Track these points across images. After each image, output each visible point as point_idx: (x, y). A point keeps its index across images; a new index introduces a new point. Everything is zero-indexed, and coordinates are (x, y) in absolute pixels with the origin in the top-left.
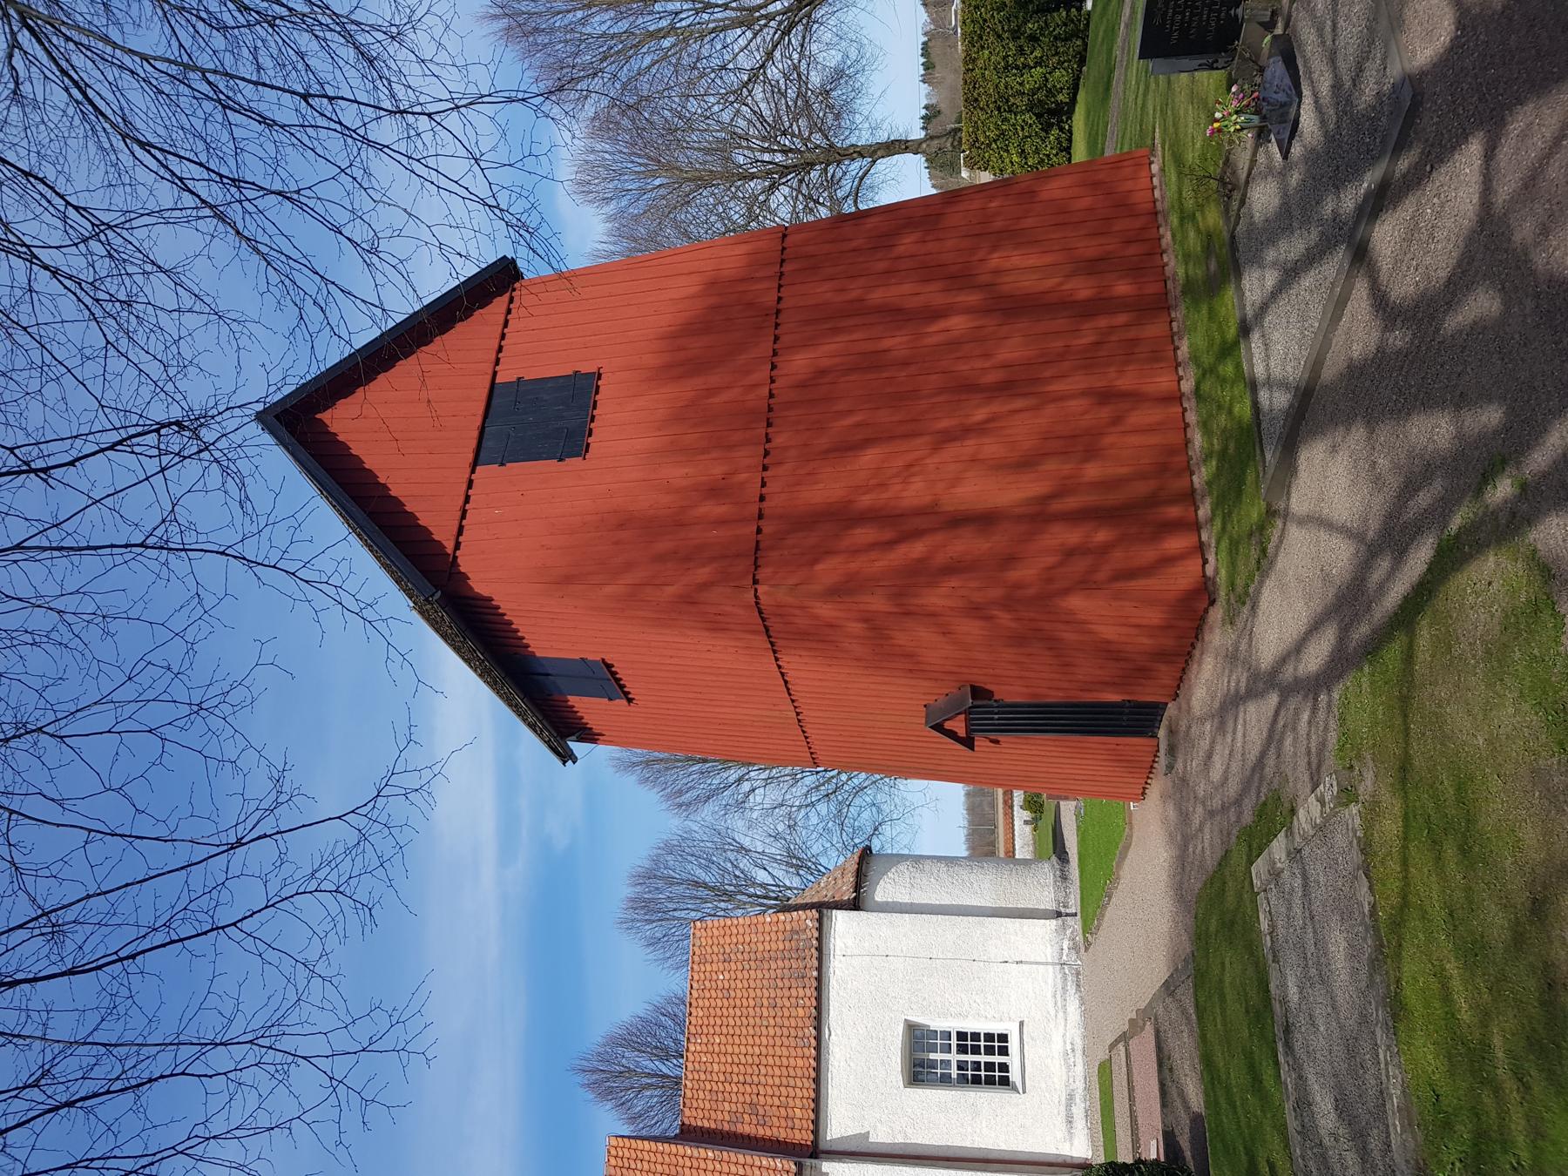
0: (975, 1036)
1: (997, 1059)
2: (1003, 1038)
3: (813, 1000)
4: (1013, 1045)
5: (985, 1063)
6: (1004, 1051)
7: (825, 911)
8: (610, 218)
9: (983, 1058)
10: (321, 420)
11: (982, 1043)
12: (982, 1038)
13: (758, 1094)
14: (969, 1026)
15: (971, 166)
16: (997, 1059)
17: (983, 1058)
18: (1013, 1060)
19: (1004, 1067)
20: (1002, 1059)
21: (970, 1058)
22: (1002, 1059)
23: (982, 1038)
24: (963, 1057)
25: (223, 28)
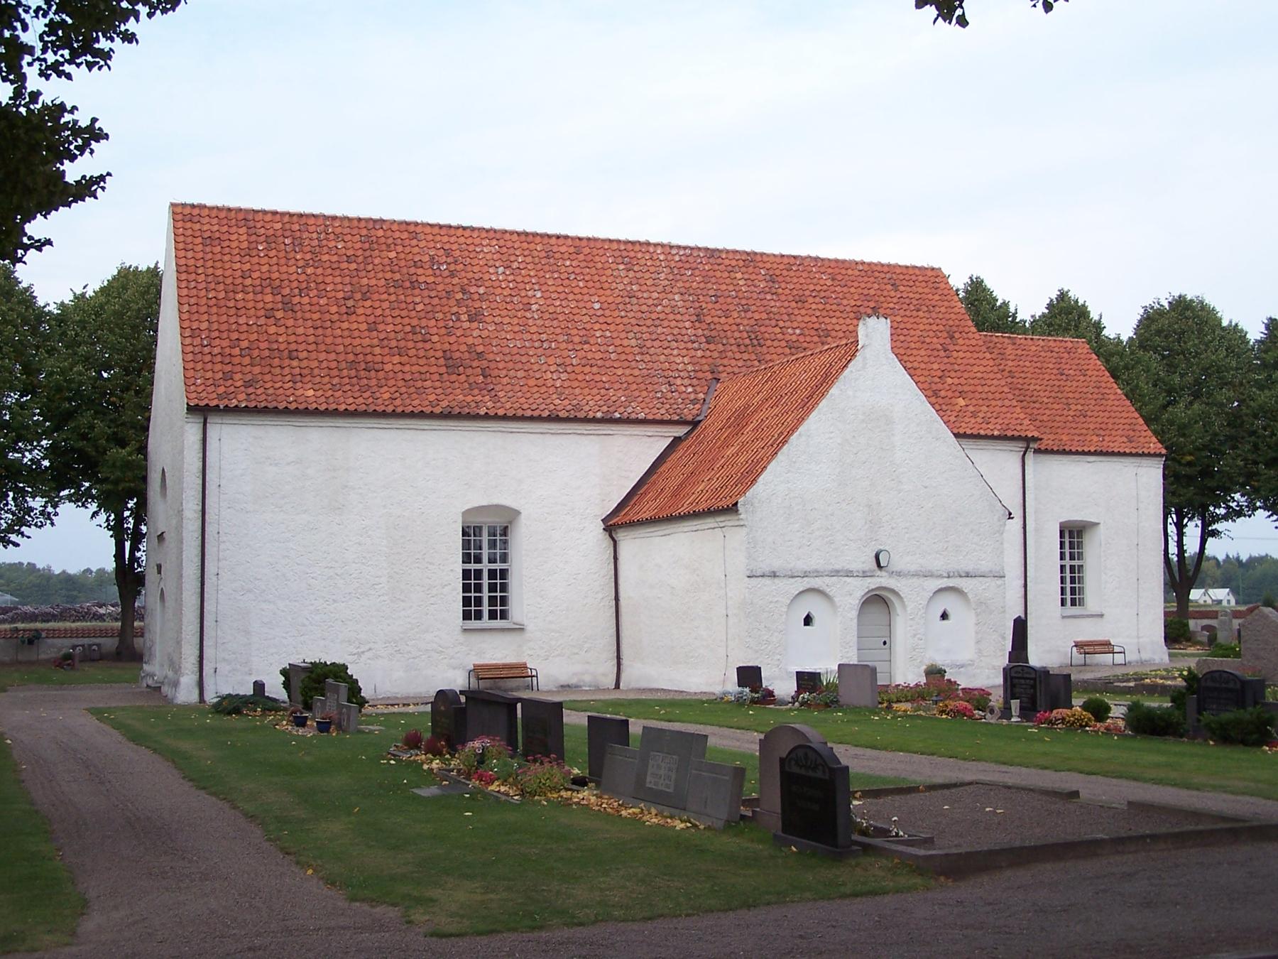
0: (466, 602)
1: (485, 608)
2: (504, 615)
3: (315, 405)
4: (498, 623)
5: (489, 592)
6: (493, 615)
7: (1164, 459)
8: (617, 533)
9: (485, 594)
10: (850, 350)
11: (498, 594)
12: (502, 594)
13: (229, 330)
14: (513, 581)
15: (65, 366)
16: (485, 608)
17: (485, 594)
18: (485, 622)
19: (479, 616)
20: (486, 614)
21: (485, 581)
22: (486, 614)
23: (502, 594)
24: (485, 575)
25: (577, 654)
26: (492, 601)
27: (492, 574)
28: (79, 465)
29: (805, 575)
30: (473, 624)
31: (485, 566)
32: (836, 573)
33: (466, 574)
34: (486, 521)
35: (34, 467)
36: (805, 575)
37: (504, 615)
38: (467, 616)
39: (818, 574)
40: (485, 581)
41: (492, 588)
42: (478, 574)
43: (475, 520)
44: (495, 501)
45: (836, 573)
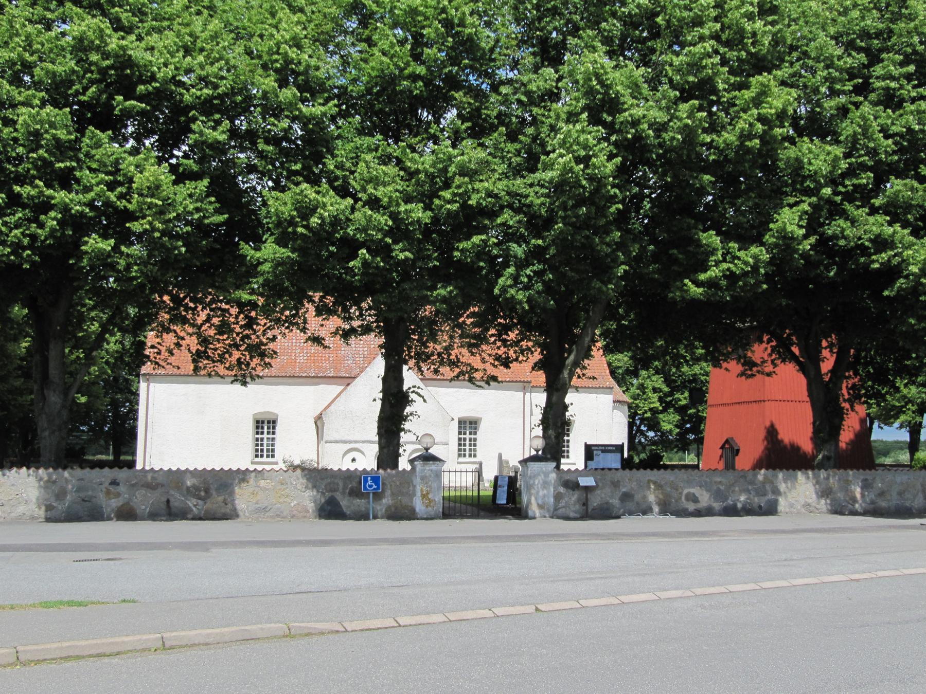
0: (459, 450)
2: (475, 456)
4: (472, 459)
9: (467, 447)
16: (265, 453)
17: (467, 447)
21: (467, 442)
26: (470, 450)
27: (470, 440)
28: (741, 182)
29: (350, 442)
30: (462, 459)
31: (468, 436)
32: (363, 442)
33: (460, 439)
34: (266, 417)
35: (183, 119)
36: (350, 442)
37: (475, 456)
38: (459, 455)
39: (356, 442)
40: (467, 442)
41: (470, 445)
42: (465, 439)
43: (260, 418)
44: (267, 410)
45: (363, 442)
